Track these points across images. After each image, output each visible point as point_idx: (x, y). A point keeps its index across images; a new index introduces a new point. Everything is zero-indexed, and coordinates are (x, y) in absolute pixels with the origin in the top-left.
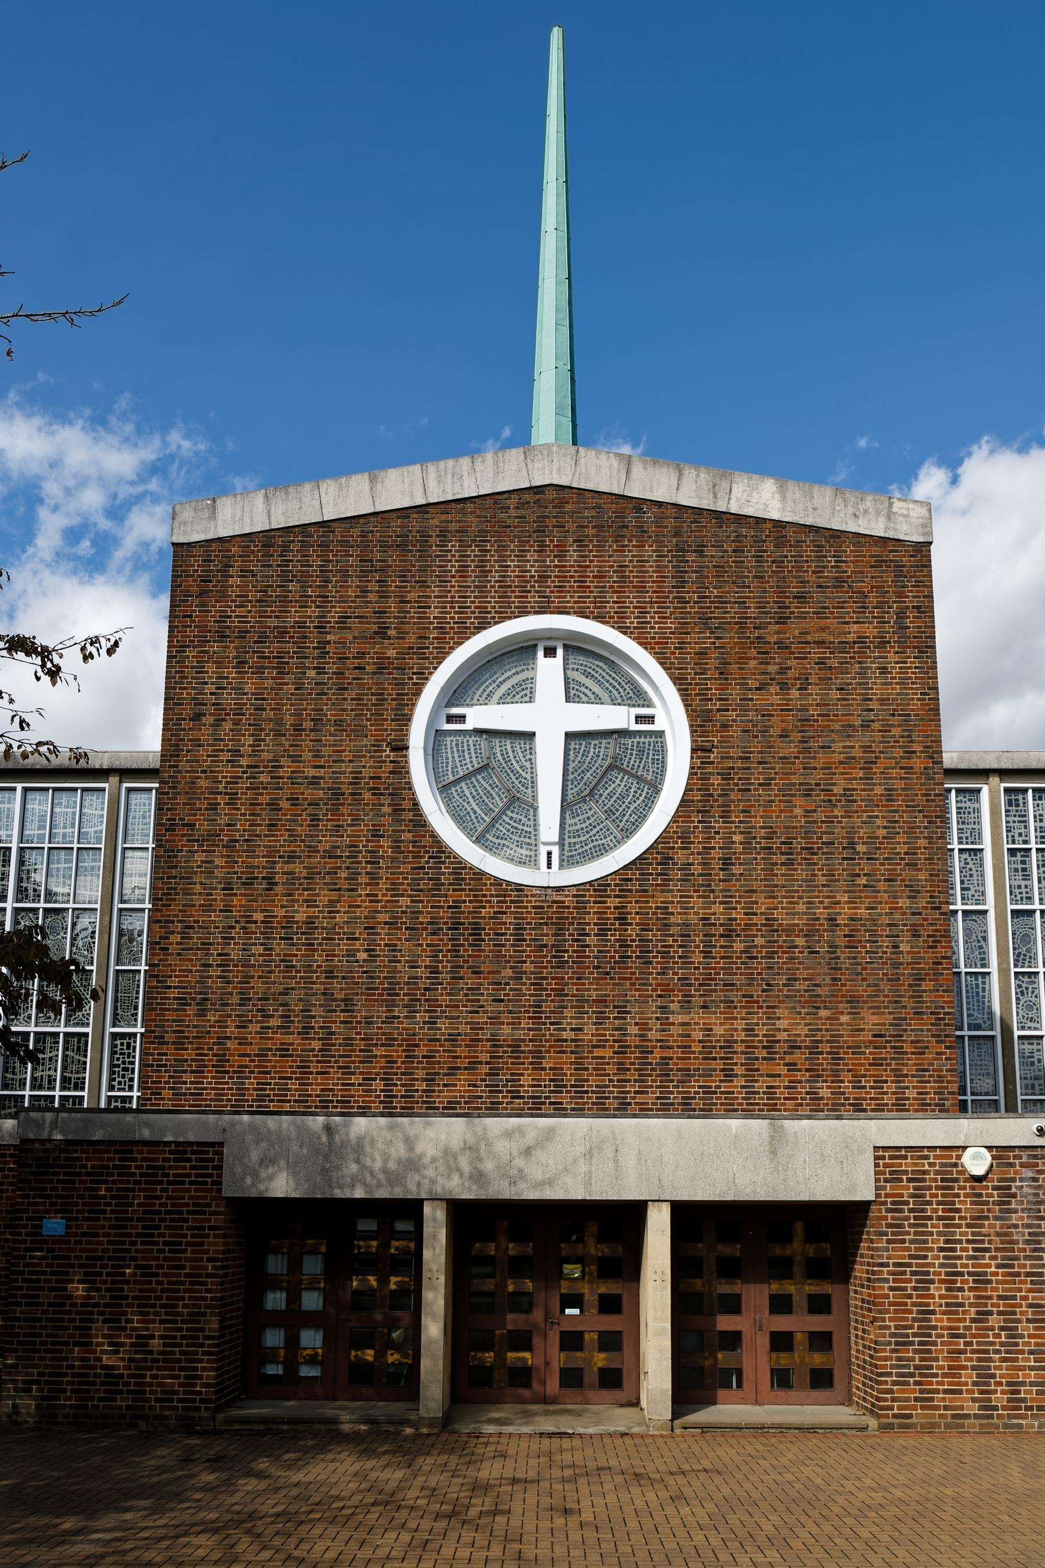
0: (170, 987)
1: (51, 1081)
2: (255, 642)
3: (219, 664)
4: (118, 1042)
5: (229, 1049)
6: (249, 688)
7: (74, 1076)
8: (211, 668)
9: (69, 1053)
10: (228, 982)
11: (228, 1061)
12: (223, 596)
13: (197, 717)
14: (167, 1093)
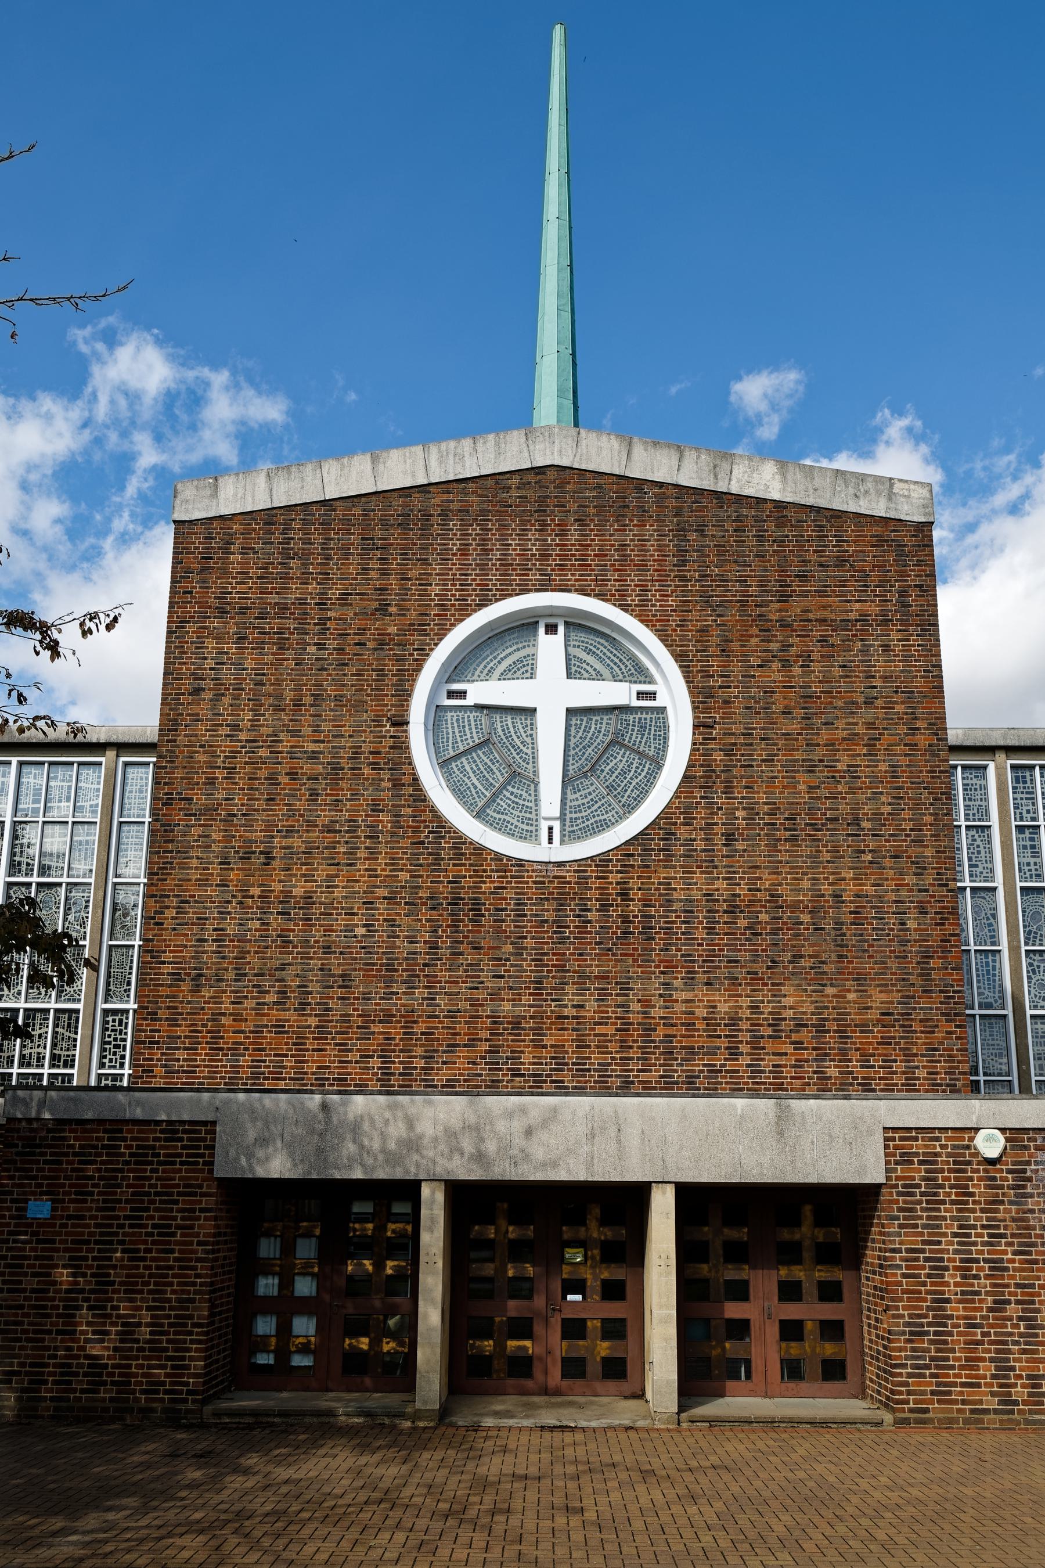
0: (164, 963)
1: (40, 1058)
2: (256, 618)
3: (219, 639)
4: (110, 1019)
5: (223, 1026)
6: (249, 663)
7: (63, 1053)
8: (211, 644)
9: (58, 1030)
10: (224, 958)
11: (222, 1037)
12: (224, 573)
13: (197, 691)
14: (159, 1071)
